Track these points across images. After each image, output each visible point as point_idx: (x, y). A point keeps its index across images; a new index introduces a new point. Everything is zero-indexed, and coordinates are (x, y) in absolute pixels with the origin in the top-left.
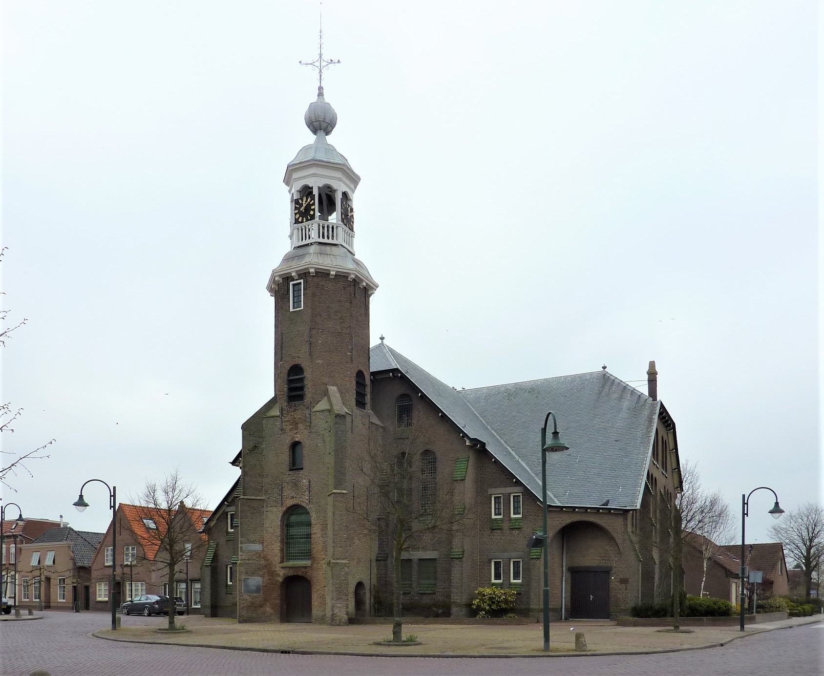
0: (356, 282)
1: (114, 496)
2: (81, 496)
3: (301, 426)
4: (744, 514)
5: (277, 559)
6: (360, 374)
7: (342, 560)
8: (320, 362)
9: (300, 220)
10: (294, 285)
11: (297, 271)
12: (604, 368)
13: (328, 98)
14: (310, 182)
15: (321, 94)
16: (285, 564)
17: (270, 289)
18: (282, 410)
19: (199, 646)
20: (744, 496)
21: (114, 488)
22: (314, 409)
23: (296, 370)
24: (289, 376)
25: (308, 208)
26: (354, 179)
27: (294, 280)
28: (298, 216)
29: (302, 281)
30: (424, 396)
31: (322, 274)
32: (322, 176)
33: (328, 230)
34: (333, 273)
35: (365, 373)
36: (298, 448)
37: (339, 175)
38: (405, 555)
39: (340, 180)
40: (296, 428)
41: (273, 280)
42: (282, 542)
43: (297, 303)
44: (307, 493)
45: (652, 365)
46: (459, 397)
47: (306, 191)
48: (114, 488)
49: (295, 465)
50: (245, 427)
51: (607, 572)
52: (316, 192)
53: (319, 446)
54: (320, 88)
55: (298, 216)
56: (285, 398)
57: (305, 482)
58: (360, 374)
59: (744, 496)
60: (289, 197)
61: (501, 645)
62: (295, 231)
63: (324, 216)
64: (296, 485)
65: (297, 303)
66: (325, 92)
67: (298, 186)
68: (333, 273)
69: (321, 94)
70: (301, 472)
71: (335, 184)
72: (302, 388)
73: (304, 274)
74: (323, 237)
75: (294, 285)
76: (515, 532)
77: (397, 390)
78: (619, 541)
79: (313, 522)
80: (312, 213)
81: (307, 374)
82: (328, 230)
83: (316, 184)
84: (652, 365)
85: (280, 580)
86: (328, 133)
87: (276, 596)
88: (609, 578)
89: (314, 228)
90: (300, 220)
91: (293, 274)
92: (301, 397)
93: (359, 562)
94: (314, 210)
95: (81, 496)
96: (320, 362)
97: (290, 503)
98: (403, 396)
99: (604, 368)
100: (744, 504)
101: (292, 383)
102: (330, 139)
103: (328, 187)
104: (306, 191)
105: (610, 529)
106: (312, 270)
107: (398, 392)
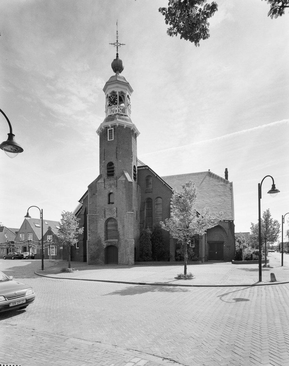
1: (42, 213)
2: (28, 213)
3: (113, 186)
4: (283, 223)
5: (103, 239)
8: (120, 161)
9: (111, 105)
11: (111, 125)
12: (209, 170)
13: (120, 58)
14: (115, 90)
15: (117, 56)
16: (106, 241)
17: (98, 132)
18: (104, 180)
19: (81, 280)
20: (283, 216)
21: (42, 210)
22: (118, 180)
23: (110, 164)
24: (107, 167)
25: (115, 100)
26: (131, 91)
27: (109, 128)
28: (110, 103)
29: (113, 129)
35: (136, 167)
36: (111, 196)
39: (117, 87)
40: (111, 187)
41: (100, 128)
42: (105, 232)
43: (111, 138)
44: (116, 213)
45: (226, 169)
47: (114, 93)
48: (42, 210)
51: (222, 243)
52: (117, 94)
53: (119, 196)
55: (110, 103)
56: (106, 175)
57: (115, 208)
59: (283, 216)
60: (105, 96)
61: (246, 287)
62: (109, 109)
63: (120, 104)
64: (111, 210)
65: (111, 138)
66: (119, 55)
68: (125, 126)
69: (117, 56)
70: (113, 204)
72: (113, 171)
75: (109, 130)
78: (227, 232)
79: (118, 224)
80: (116, 102)
81: (115, 165)
83: (118, 91)
84: (226, 169)
85: (105, 247)
86: (120, 72)
87: (102, 254)
88: (223, 245)
89: (116, 108)
90: (111, 105)
91: (110, 126)
92: (113, 175)
94: (117, 101)
95: (28, 213)
96: (120, 161)
97: (108, 217)
99: (209, 170)
100: (283, 219)
101: (109, 170)
102: (120, 75)
103: (122, 92)
104: (114, 93)
106: (117, 124)
107: (145, 175)
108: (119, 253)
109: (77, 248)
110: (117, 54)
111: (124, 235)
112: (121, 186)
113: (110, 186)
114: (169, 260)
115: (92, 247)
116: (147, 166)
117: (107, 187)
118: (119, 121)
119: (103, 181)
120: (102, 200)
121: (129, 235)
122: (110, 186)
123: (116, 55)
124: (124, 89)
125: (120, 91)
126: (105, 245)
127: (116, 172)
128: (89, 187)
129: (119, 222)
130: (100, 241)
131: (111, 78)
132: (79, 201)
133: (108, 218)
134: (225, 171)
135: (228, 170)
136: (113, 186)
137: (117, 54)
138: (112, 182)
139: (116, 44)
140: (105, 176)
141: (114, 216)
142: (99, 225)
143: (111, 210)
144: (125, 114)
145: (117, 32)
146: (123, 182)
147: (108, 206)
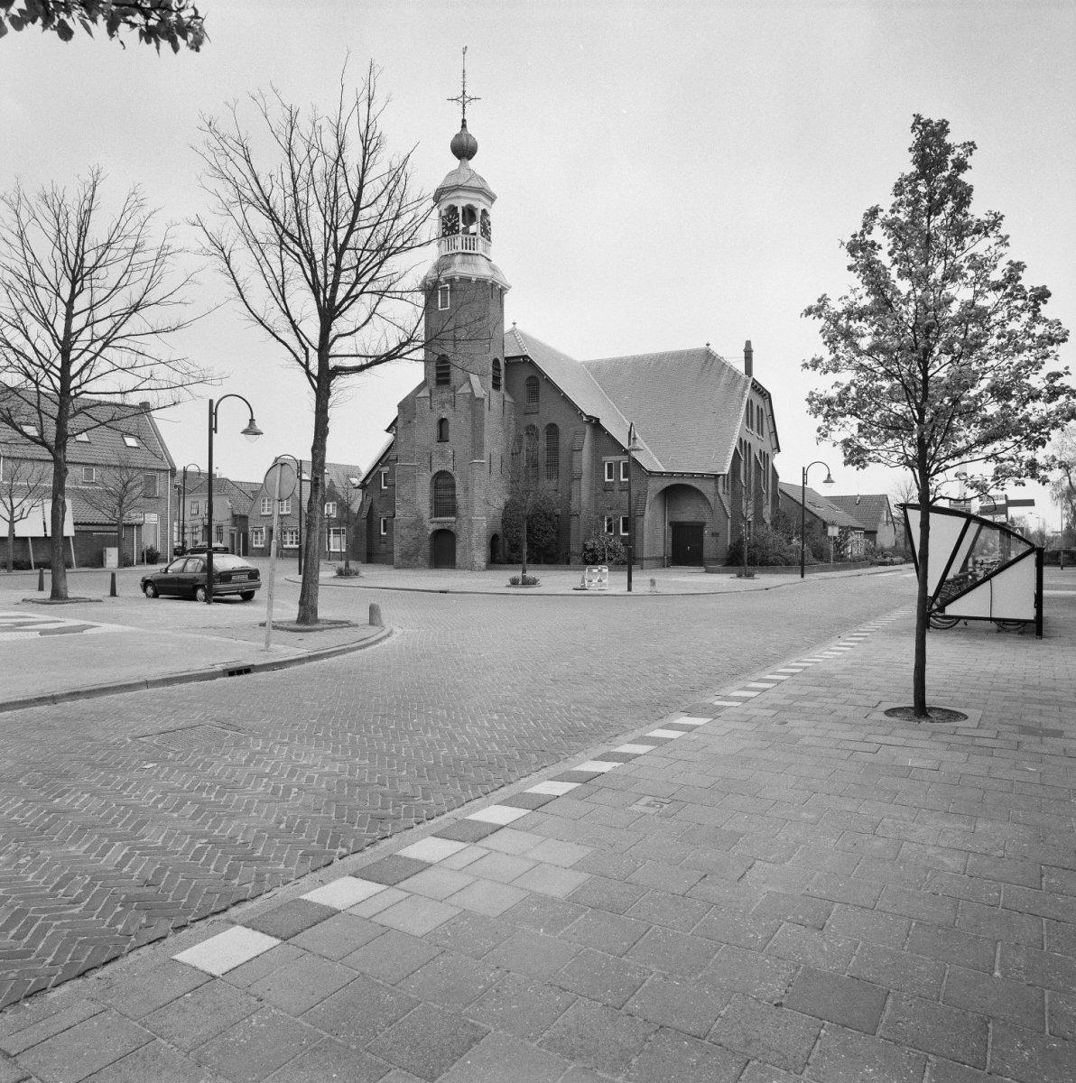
0: (493, 285)
3: (447, 406)
5: (426, 516)
6: (496, 362)
13: (470, 130)
14: (455, 203)
15: (464, 126)
18: (431, 392)
29: (448, 285)
30: (548, 380)
34: (474, 280)
37: (461, 193)
39: (458, 197)
45: (748, 343)
49: (442, 437)
58: (496, 362)
59: (804, 468)
64: (442, 455)
66: (468, 124)
69: (464, 126)
72: (448, 374)
77: (523, 375)
84: (748, 343)
86: (470, 159)
92: (447, 382)
97: (436, 470)
99: (708, 345)
100: (804, 474)
107: (524, 377)
108: (458, 546)
109: (382, 533)
110: (464, 121)
111: (467, 508)
112: (462, 405)
113: (442, 404)
114: (568, 563)
115: (404, 532)
116: (527, 356)
117: (436, 406)
118: (459, 269)
119: (428, 395)
120: (426, 432)
121: (483, 505)
122: (442, 404)
123: (461, 124)
124: (472, 199)
125: (464, 205)
126: (431, 528)
127: (456, 375)
128: (401, 406)
129: (457, 480)
130: (420, 520)
131: (447, 176)
132: (388, 431)
133: (437, 470)
134: (744, 346)
135: (753, 347)
136: (447, 406)
137: (464, 121)
138: (445, 396)
139: (359, 253)
140: (432, 383)
141: (449, 468)
142: (419, 486)
143: (442, 455)
144: (475, 252)
145: (464, 71)
146: (468, 396)
147: (436, 447)
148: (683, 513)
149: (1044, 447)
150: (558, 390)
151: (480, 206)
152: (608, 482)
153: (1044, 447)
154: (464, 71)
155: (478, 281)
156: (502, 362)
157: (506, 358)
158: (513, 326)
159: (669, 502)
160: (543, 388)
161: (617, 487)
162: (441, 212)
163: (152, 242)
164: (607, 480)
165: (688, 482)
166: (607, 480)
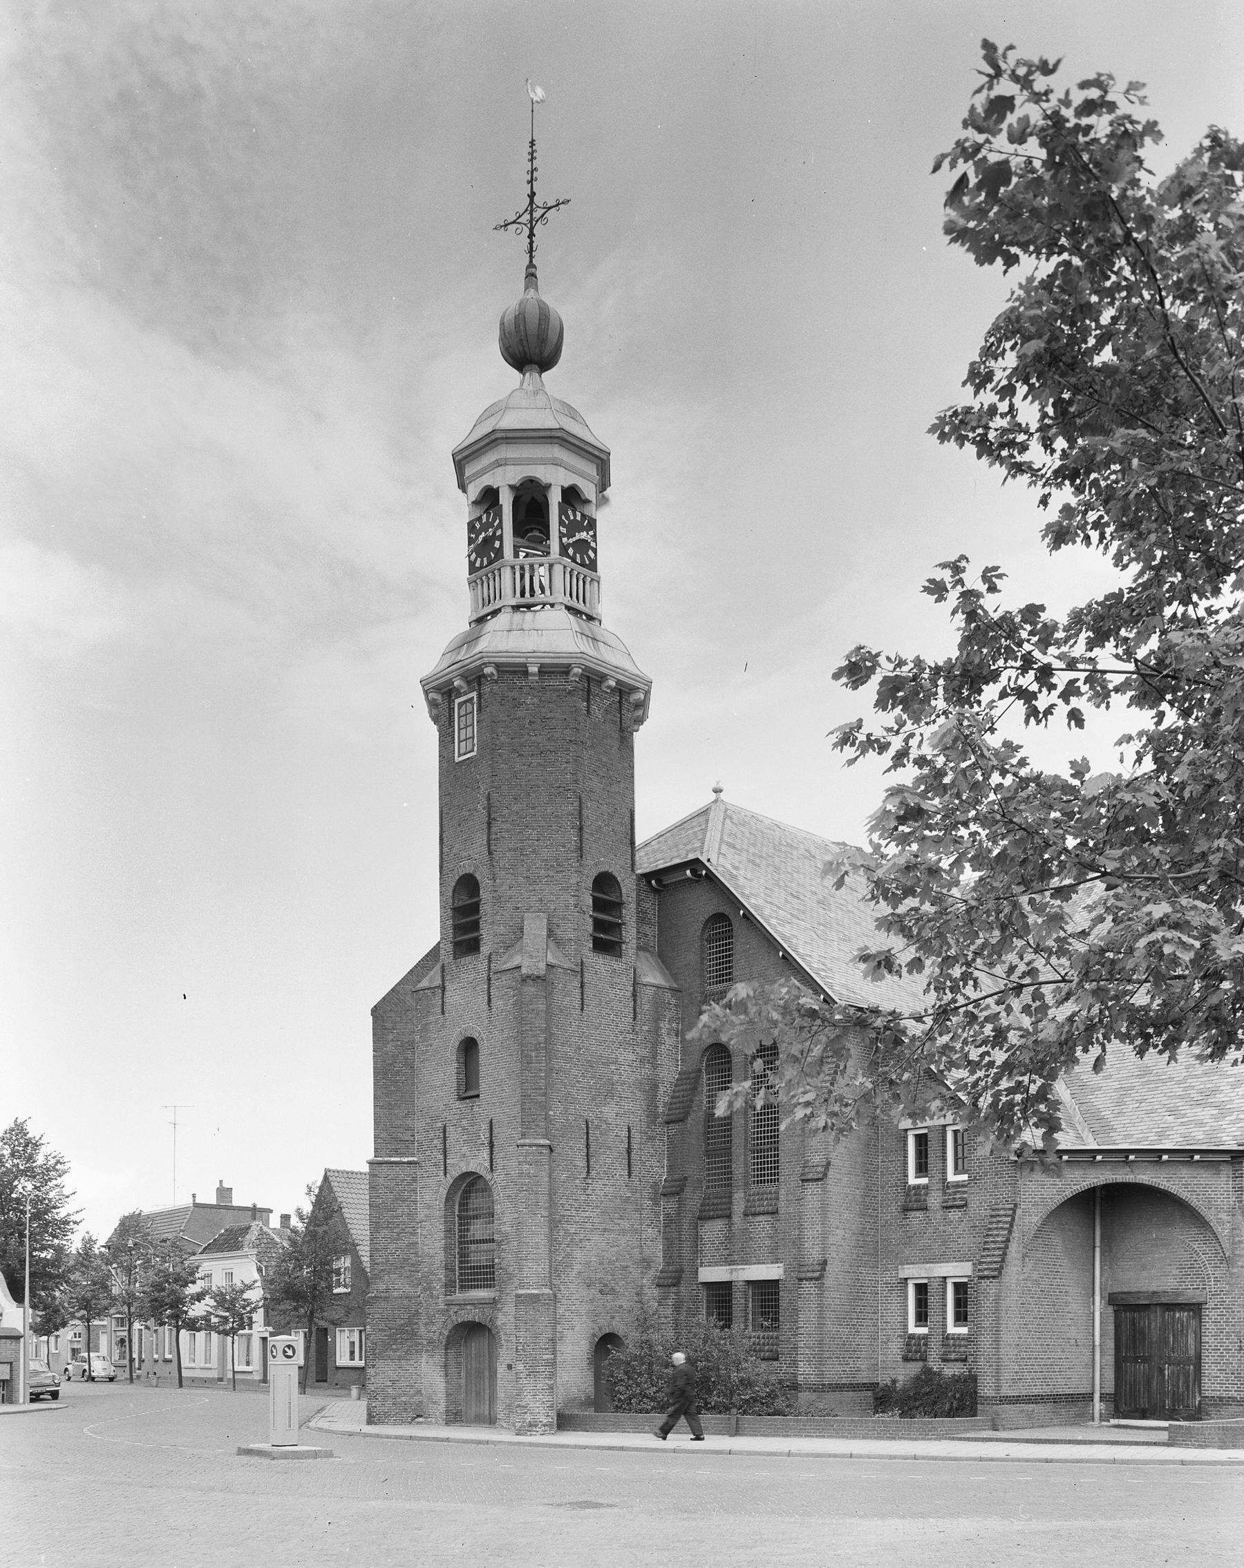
0: (593, 679)
6: (604, 882)
7: (583, 1252)
10: (460, 705)
27: (459, 695)
30: (748, 917)
31: (513, 671)
32: (517, 462)
33: (522, 576)
34: (533, 669)
37: (557, 452)
38: (710, 1274)
39: (556, 463)
46: (153, 1217)
49: (468, 1089)
50: (375, 1011)
54: (531, 265)
58: (604, 882)
67: (474, 490)
71: (543, 474)
73: (475, 678)
74: (523, 595)
76: (954, 1215)
77: (702, 905)
80: (497, 544)
82: (522, 576)
83: (505, 479)
93: (916, 856)
97: (454, 1173)
98: (719, 918)
105: (1184, 1194)
145: (532, 143)
148: (1144, 1268)
149: (1042, 608)
150: (771, 943)
151: (556, 479)
152: (917, 1187)
153: (1042, 608)
154: (532, 143)
155: (544, 670)
156: (628, 888)
157: (647, 876)
158: (713, 796)
159: (1107, 1240)
160: (742, 941)
161: (934, 1200)
162: (1072, 646)
163: (989, 1212)
164: (913, 1180)
165: (1145, 1177)
166: (913, 1180)
